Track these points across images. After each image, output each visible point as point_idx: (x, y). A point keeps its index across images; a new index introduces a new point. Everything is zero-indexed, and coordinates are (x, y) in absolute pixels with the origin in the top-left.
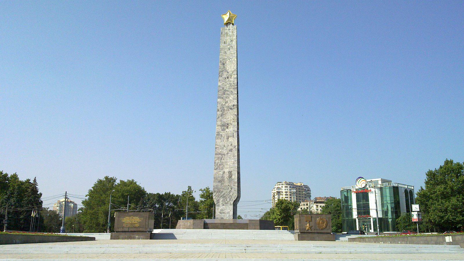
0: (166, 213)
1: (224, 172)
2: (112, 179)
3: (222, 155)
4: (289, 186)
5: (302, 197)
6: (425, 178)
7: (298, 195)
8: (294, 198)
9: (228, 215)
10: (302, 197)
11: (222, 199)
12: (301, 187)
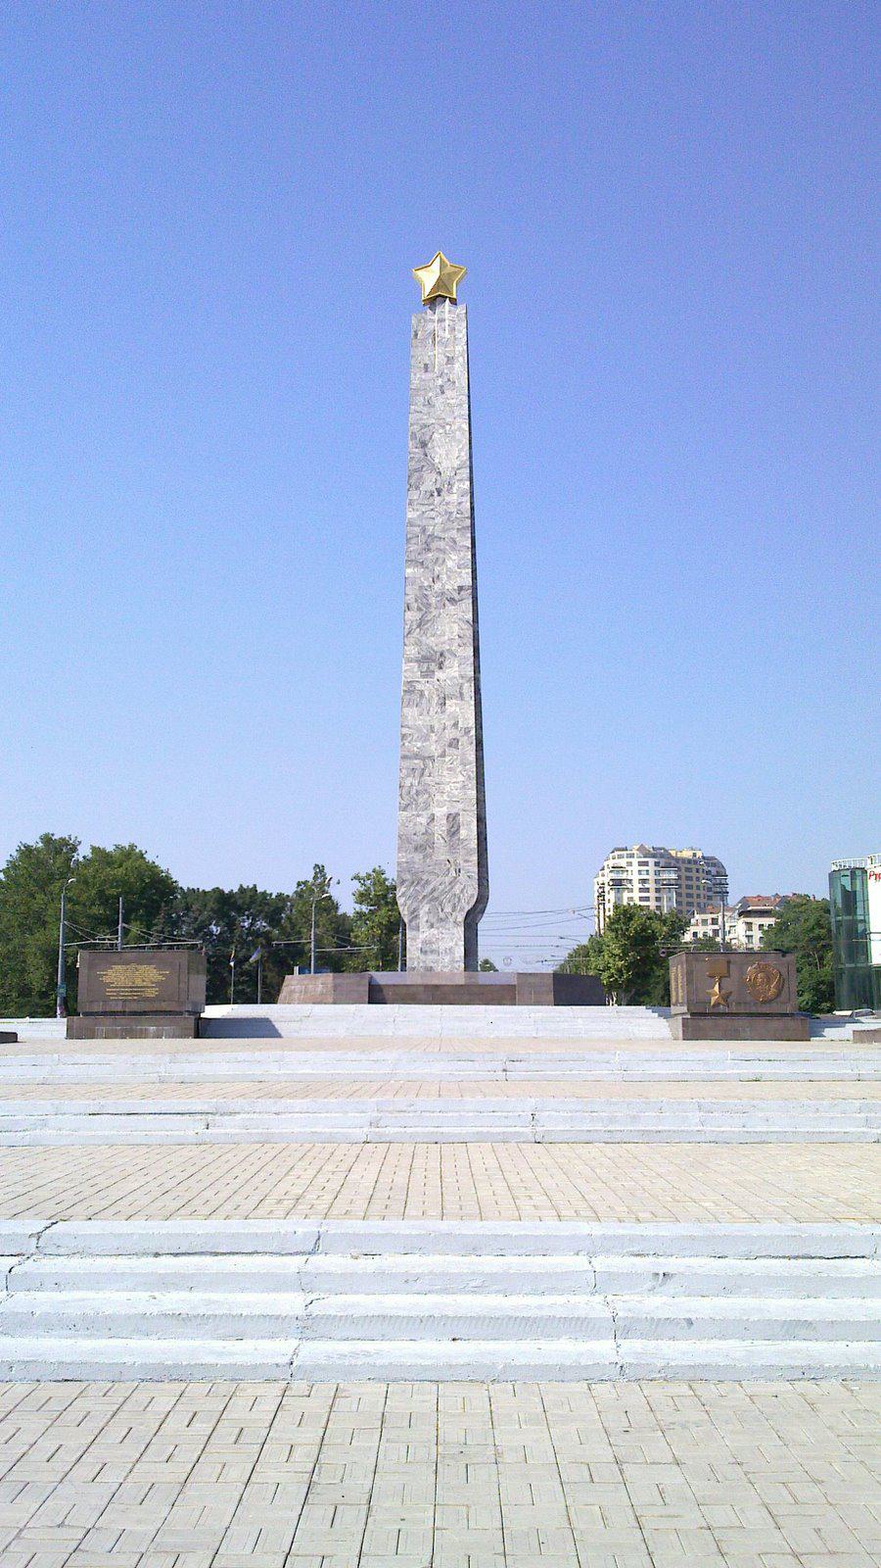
3: (423, 759)
4: (651, 861)
7: (684, 891)
8: (670, 899)
9: (447, 959)
11: (426, 908)
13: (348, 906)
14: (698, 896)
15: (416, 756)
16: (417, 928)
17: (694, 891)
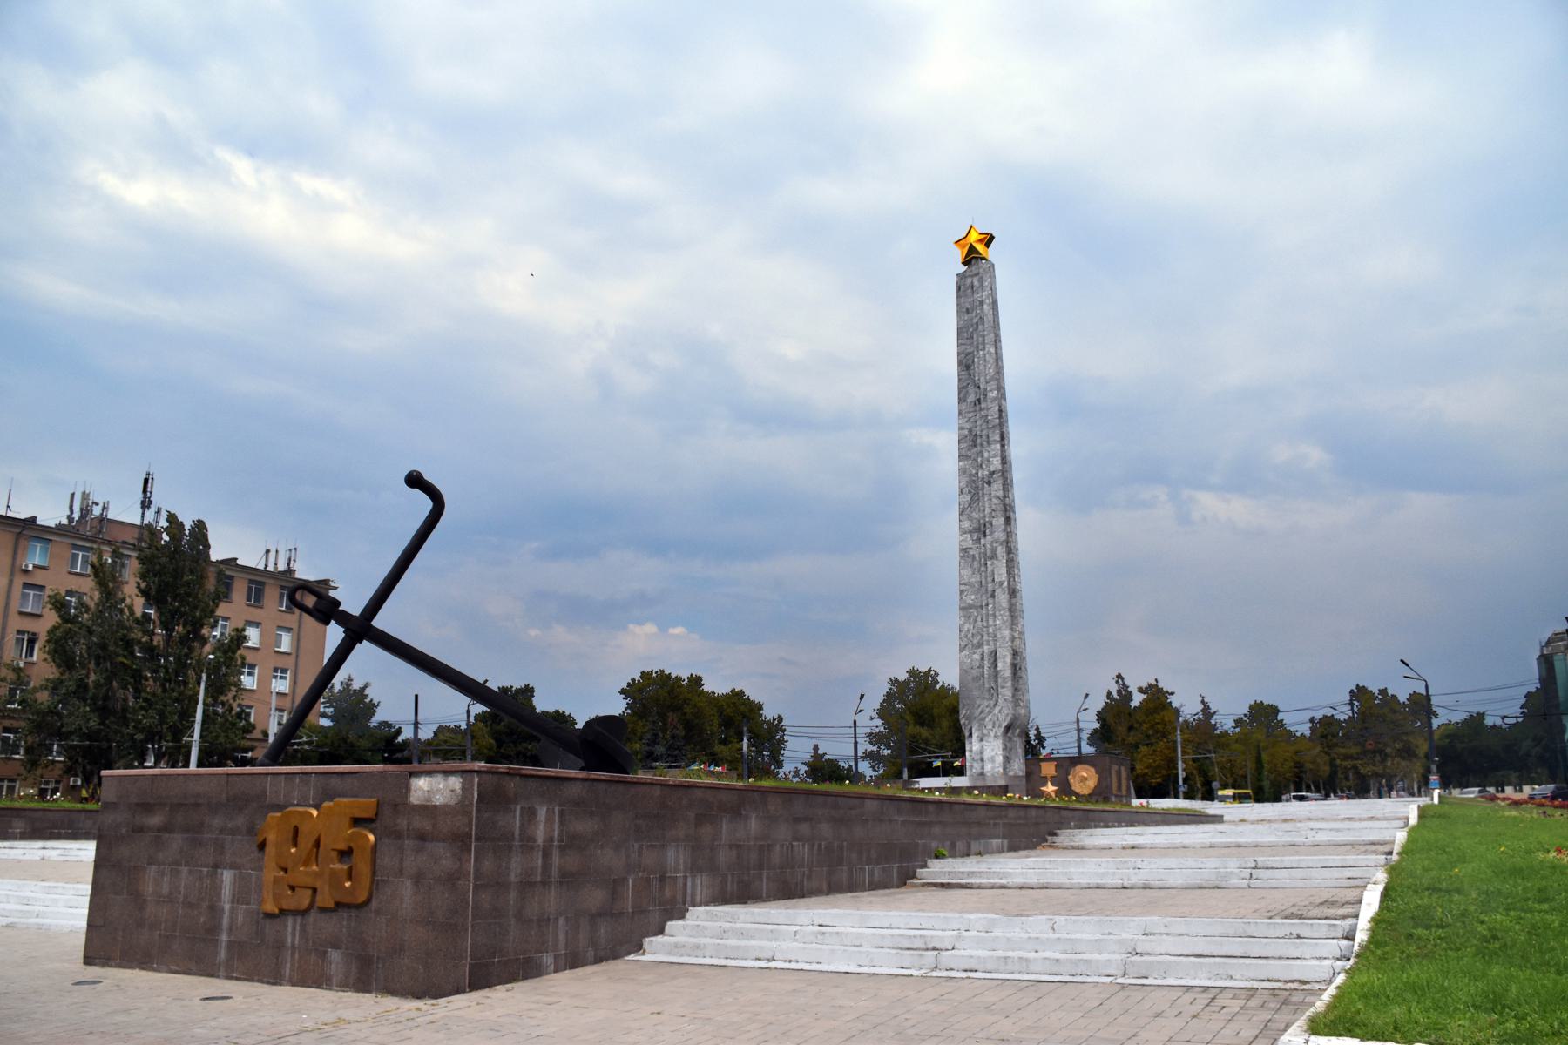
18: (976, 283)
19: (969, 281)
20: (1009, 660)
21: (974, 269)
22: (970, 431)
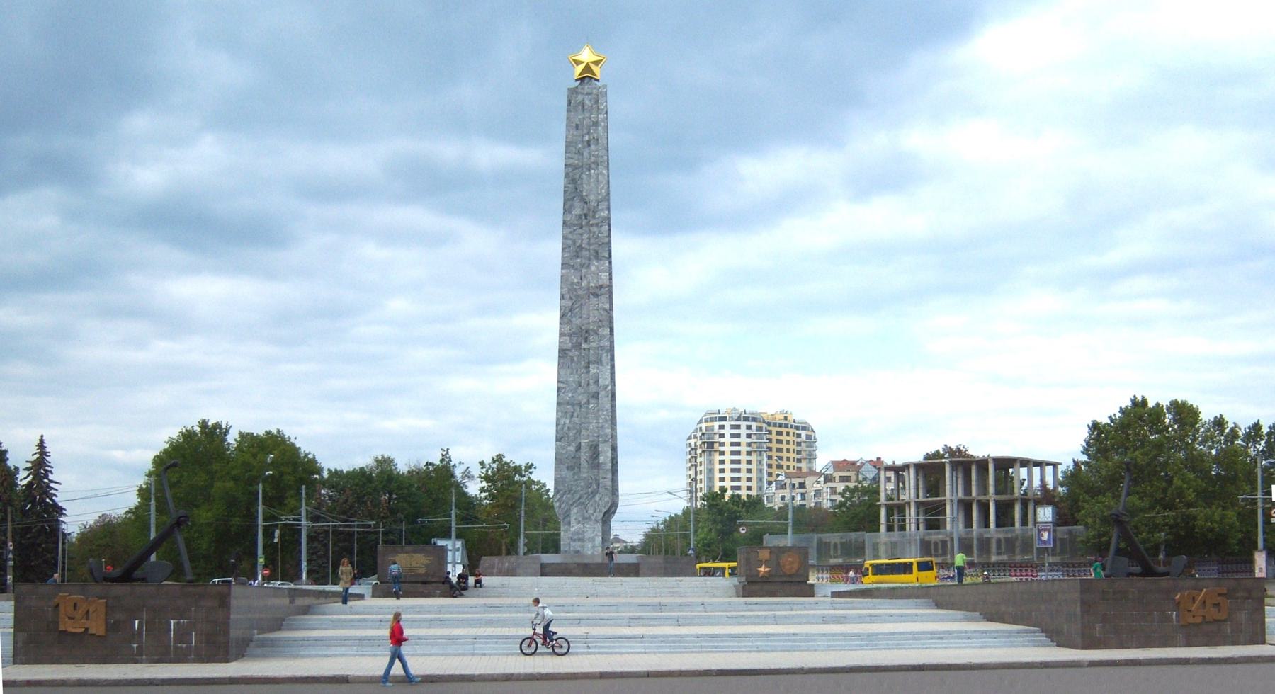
0: (401, 526)
1: (579, 448)
2: (217, 426)
3: (573, 405)
4: (743, 424)
5: (788, 450)
6: (1084, 433)
7: (774, 454)
8: (760, 462)
9: (590, 545)
10: (788, 450)
11: (575, 510)
12: (786, 426)
13: (474, 488)
14: (788, 459)
15: (568, 403)
16: (569, 523)
17: (784, 446)
18: (588, 102)
19: (580, 98)
20: (609, 454)
21: (587, 88)
22: (574, 242)
